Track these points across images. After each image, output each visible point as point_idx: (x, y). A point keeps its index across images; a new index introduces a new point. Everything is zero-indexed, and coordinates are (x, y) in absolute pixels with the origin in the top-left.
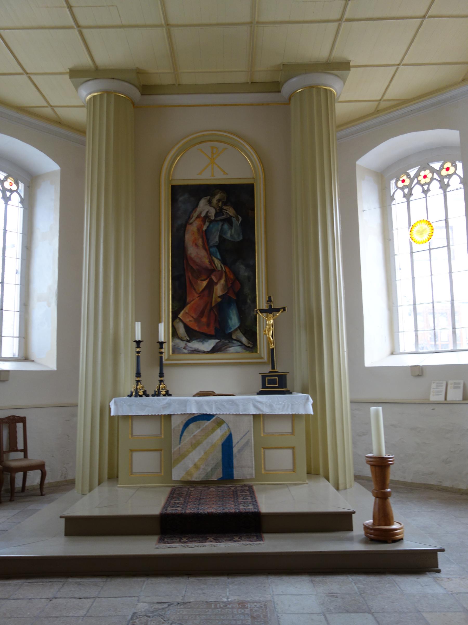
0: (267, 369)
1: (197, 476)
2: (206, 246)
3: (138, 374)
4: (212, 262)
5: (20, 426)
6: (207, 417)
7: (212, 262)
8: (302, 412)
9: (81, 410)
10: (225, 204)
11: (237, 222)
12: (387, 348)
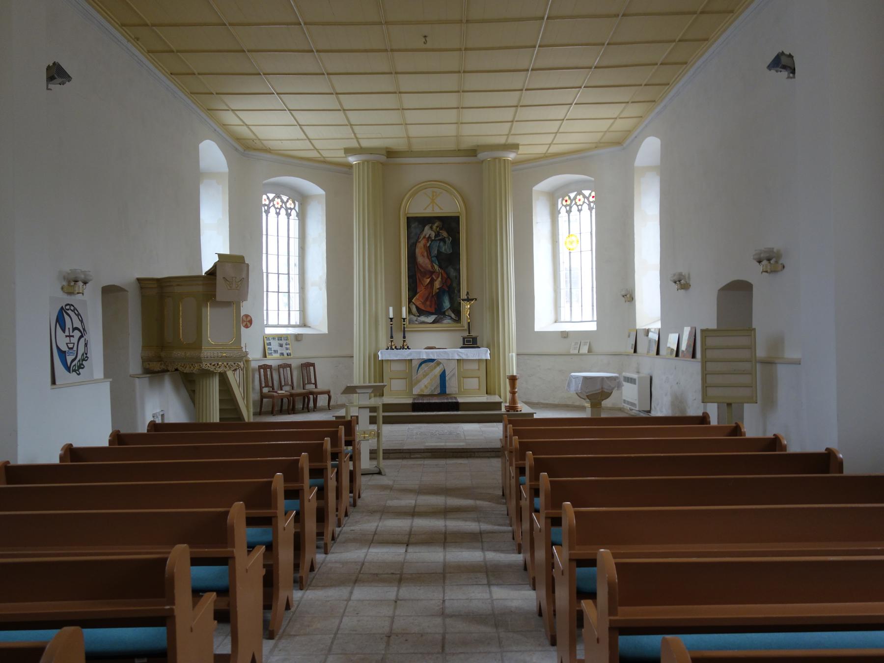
0: (466, 334)
1: (426, 392)
2: (429, 256)
3: (392, 337)
4: (433, 267)
5: (312, 368)
6: (432, 360)
7: (433, 267)
8: (484, 358)
9: (356, 360)
10: (441, 229)
11: (448, 242)
12: (551, 316)
